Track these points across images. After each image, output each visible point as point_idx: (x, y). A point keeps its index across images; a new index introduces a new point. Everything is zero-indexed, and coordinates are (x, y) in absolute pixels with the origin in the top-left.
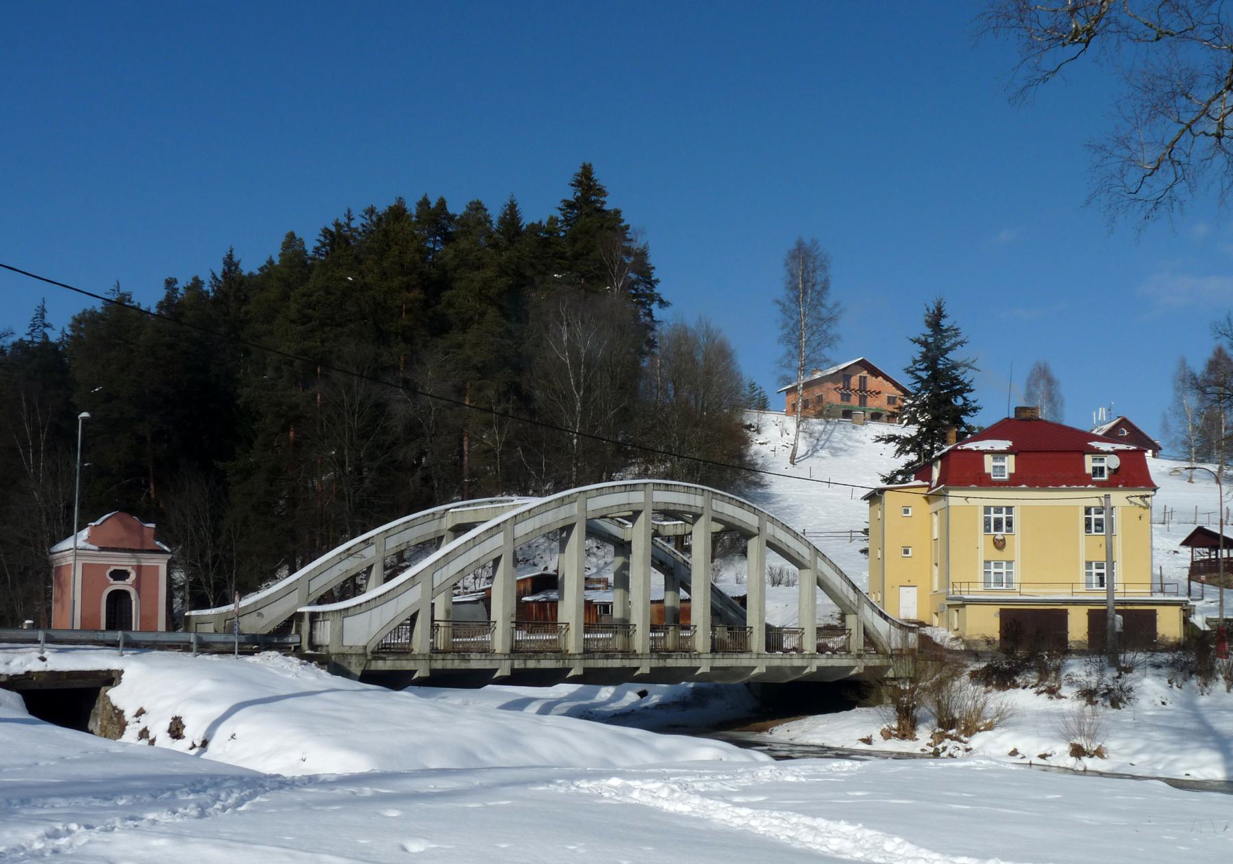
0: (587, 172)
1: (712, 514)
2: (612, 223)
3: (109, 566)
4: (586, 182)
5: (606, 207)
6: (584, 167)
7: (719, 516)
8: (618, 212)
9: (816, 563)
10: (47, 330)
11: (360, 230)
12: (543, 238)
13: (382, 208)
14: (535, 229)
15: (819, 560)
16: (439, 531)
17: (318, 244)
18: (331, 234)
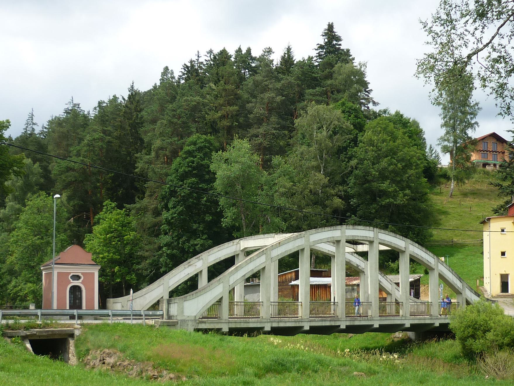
0: (331, 27)
1: (379, 241)
2: (345, 56)
3: (70, 273)
4: (330, 33)
5: (342, 47)
6: (329, 25)
7: (383, 242)
8: (348, 51)
9: (438, 266)
10: (34, 127)
11: (205, 63)
12: (307, 66)
13: (216, 51)
14: (301, 64)
15: (439, 264)
16: (236, 251)
17: (181, 74)
18: (187, 67)
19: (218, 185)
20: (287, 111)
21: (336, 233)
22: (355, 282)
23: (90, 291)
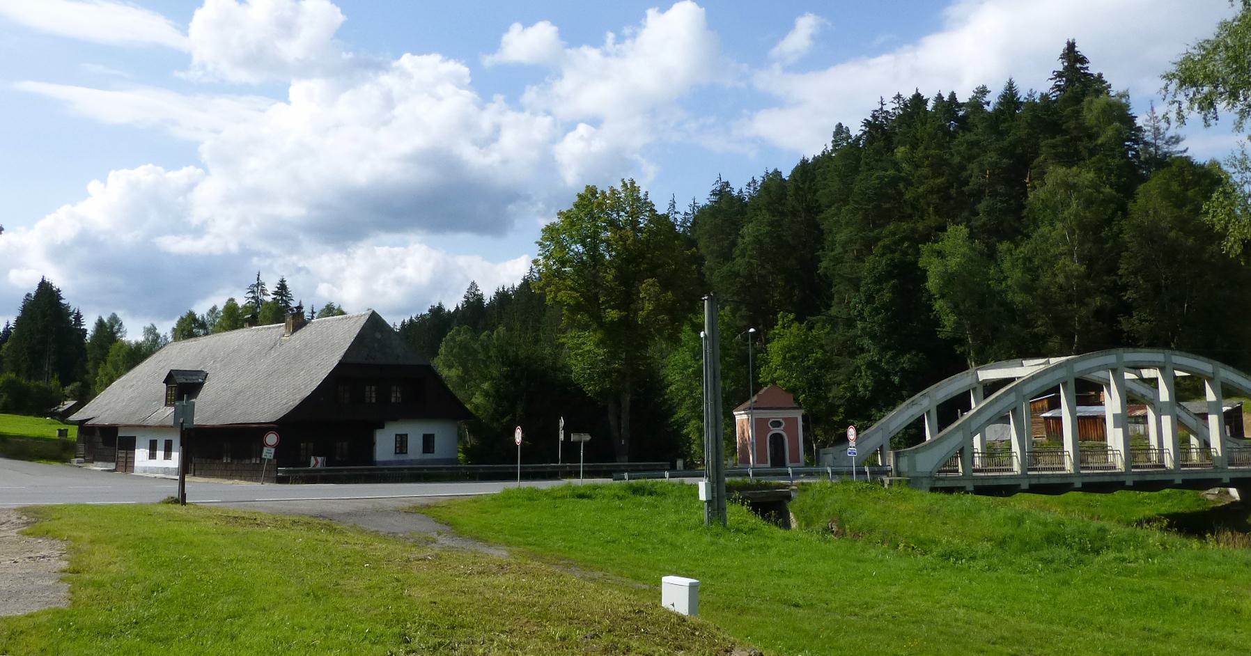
2: (1096, 85)
8: (1100, 75)
19: (932, 284)
20: (1017, 170)
21: (1111, 358)
22: (1139, 413)
23: (794, 439)
